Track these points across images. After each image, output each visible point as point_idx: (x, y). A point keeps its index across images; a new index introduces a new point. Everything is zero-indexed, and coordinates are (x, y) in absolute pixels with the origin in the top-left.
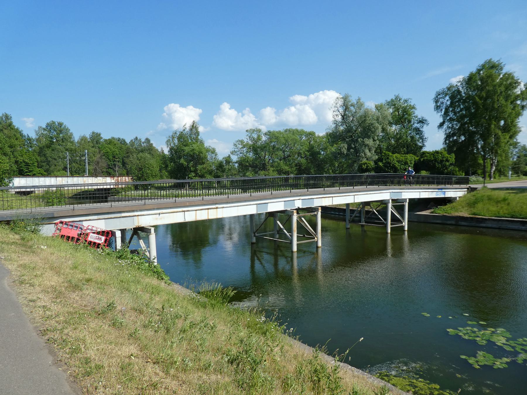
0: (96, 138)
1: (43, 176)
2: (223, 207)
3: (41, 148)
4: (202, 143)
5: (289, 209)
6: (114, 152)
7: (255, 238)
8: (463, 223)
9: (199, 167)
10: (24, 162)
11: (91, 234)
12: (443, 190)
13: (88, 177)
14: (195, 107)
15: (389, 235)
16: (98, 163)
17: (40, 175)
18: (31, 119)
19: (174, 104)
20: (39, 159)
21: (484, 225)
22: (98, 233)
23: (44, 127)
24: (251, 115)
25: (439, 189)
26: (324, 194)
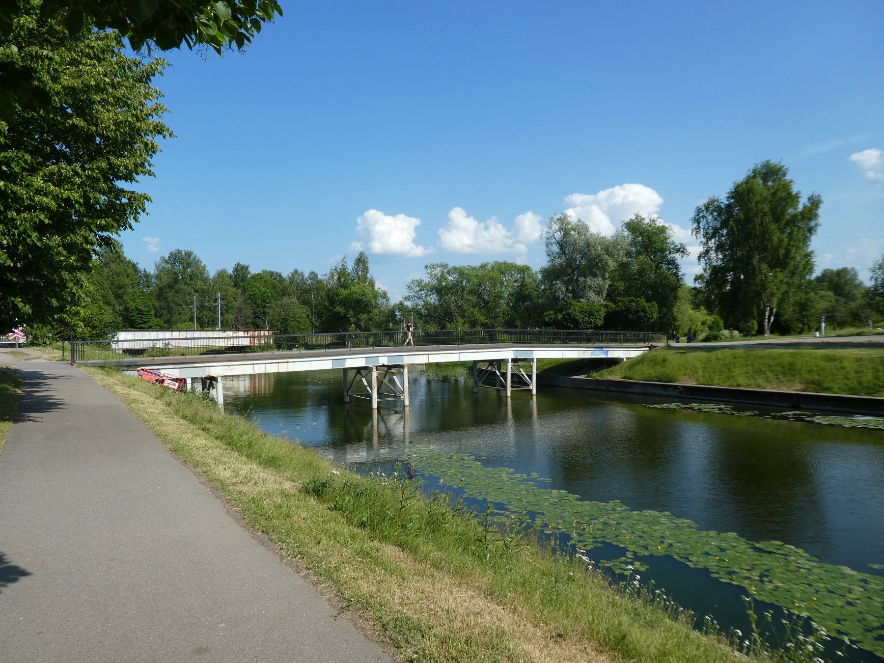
0: (240, 274)
1: (162, 329)
2: (294, 362)
3: (160, 289)
4: (372, 284)
5: (370, 366)
6: (264, 293)
7: (348, 397)
8: (613, 389)
9: (364, 317)
10: (137, 309)
11: (167, 380)
12: (604, 349)
13: (219, 331)
14: (409, 214)
15: (509, 399)
16: (240, 310)
17: (158, 327)
18: (156, 240)
19: (375, 211)
20: (157, 304)
21: (630, 390)
22: (173, 380)
23: (167, 258)
24: (500, 226)
25: (595, 348)
26: (417, 351)
